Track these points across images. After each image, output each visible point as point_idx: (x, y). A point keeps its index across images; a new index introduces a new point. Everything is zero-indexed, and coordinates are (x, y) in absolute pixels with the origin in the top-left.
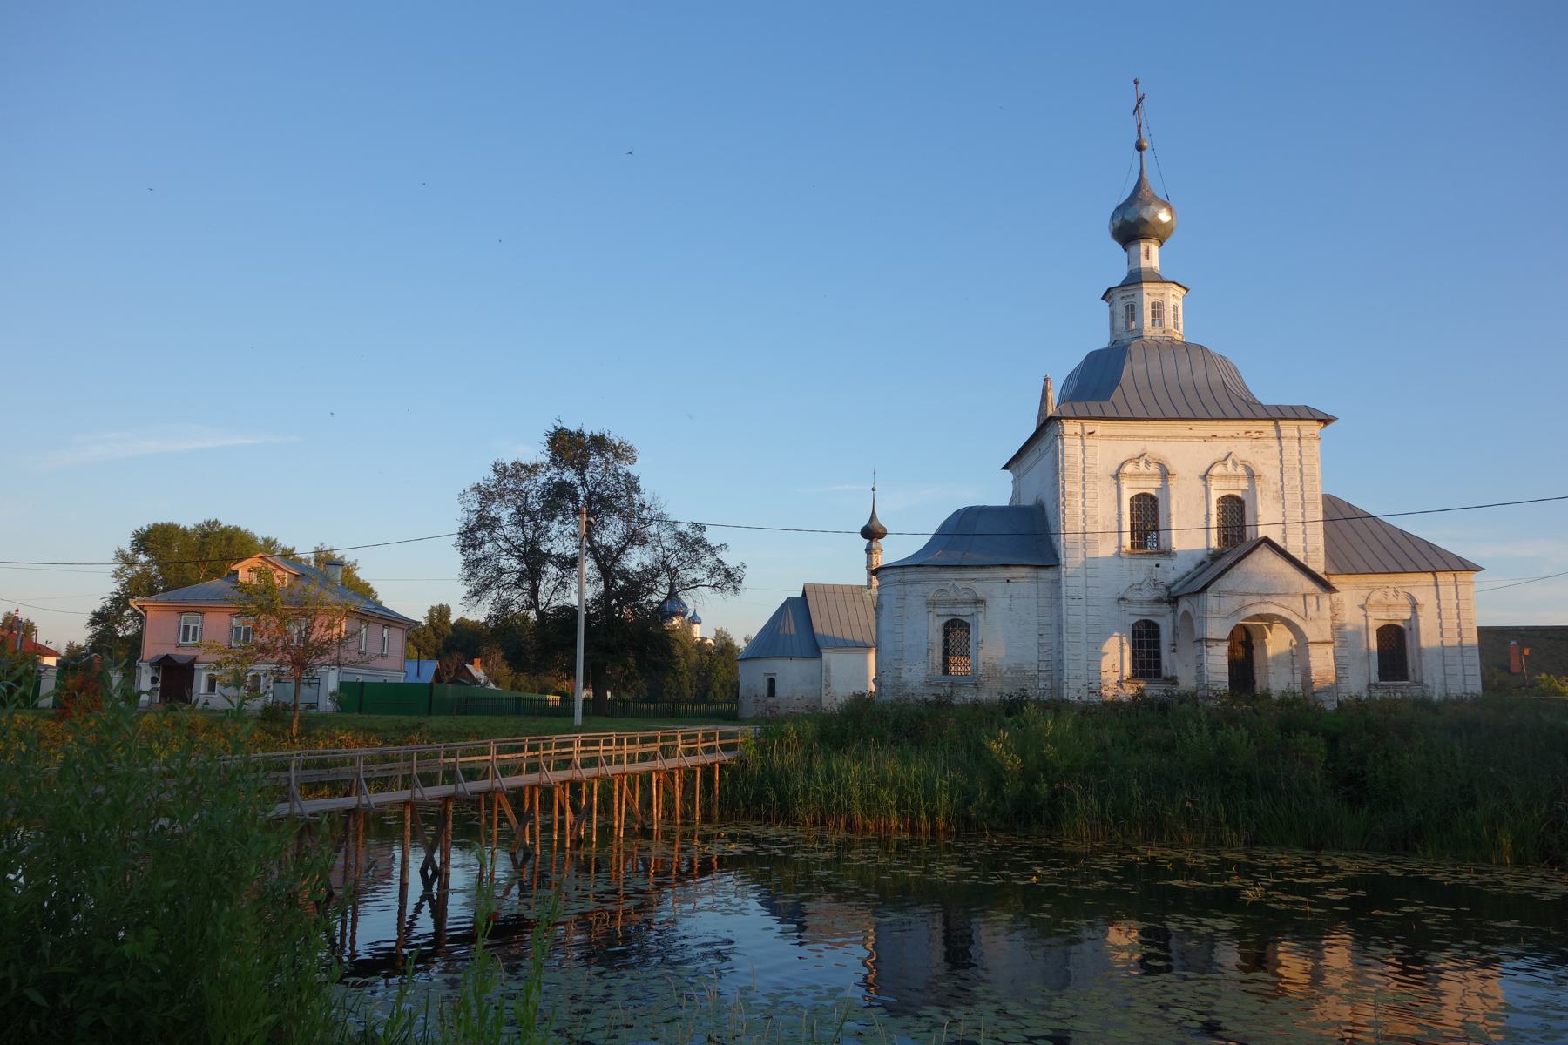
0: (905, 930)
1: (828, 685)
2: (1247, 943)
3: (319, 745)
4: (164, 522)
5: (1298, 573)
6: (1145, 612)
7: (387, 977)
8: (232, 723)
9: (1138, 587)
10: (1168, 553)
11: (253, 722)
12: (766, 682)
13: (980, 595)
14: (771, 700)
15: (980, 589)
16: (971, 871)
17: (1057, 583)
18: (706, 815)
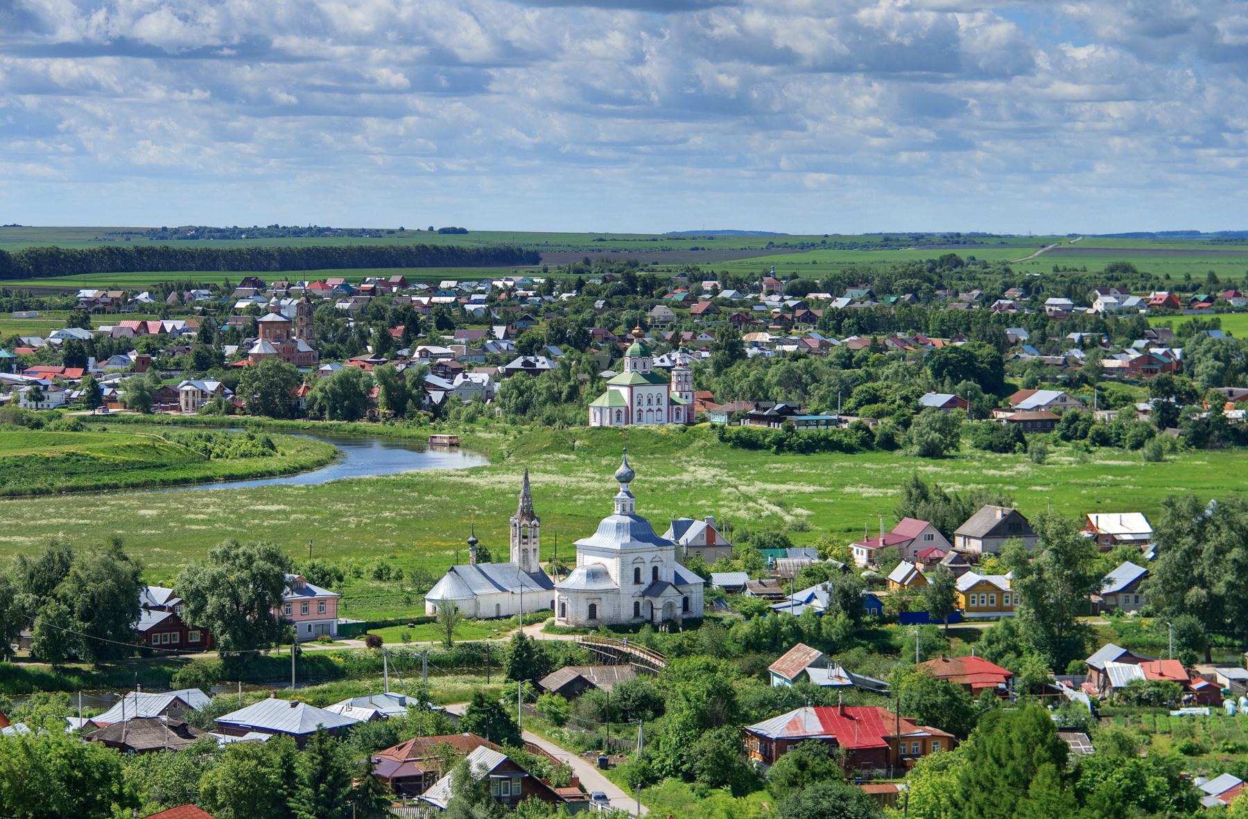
2: (1036, 491)
3: (68, 633)
4: (199, 248)
5: (562, 9)
6: (636, 599)
7: (601, 428)
8: (32, 630)
11: (417, 50)
12: (633, 606)
14: (439, 620)
16: (476, 471)
18: (380, 717)
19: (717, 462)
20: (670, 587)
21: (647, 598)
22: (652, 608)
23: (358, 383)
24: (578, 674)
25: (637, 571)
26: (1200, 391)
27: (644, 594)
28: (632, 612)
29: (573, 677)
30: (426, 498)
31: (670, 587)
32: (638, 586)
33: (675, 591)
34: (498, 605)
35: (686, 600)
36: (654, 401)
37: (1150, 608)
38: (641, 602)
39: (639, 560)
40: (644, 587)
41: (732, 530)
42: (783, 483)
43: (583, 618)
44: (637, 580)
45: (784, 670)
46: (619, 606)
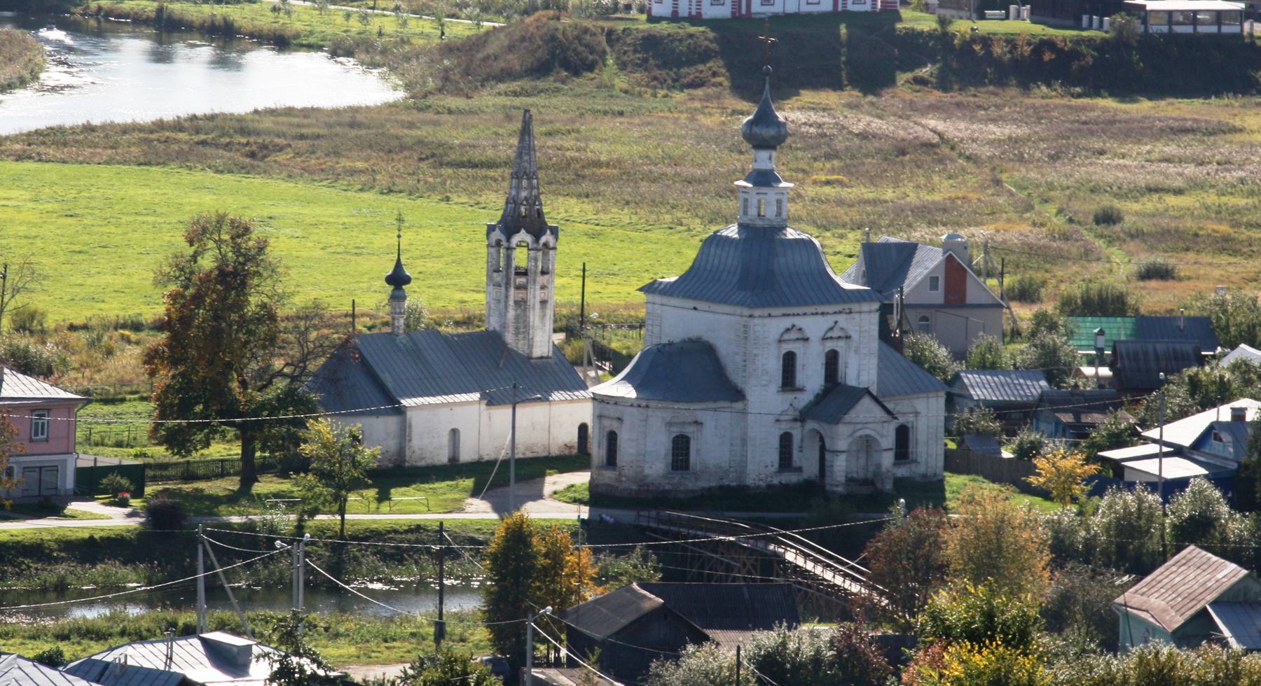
0: (26, 237)
1: (410, 440)
6: (785, 427)
9: (783, 413)
10: (801, 390)
12: (775, 443)
13: (699, 420)
15: (701, 416)
17: (744, 412)
20: (866, 402)
21: (811, 425)
22: (823, 449)
25: (789, 361)
26: (617, 92)
27: (803, 416)
28: (773, 457)
31: (866, 402)
32: (790, 396)
33: (878, 413)
35: (903, 434)
37: (360, 187)
38: (797, 434)
39: (793, 335)
40: (805, 399)
44: (789, 380)
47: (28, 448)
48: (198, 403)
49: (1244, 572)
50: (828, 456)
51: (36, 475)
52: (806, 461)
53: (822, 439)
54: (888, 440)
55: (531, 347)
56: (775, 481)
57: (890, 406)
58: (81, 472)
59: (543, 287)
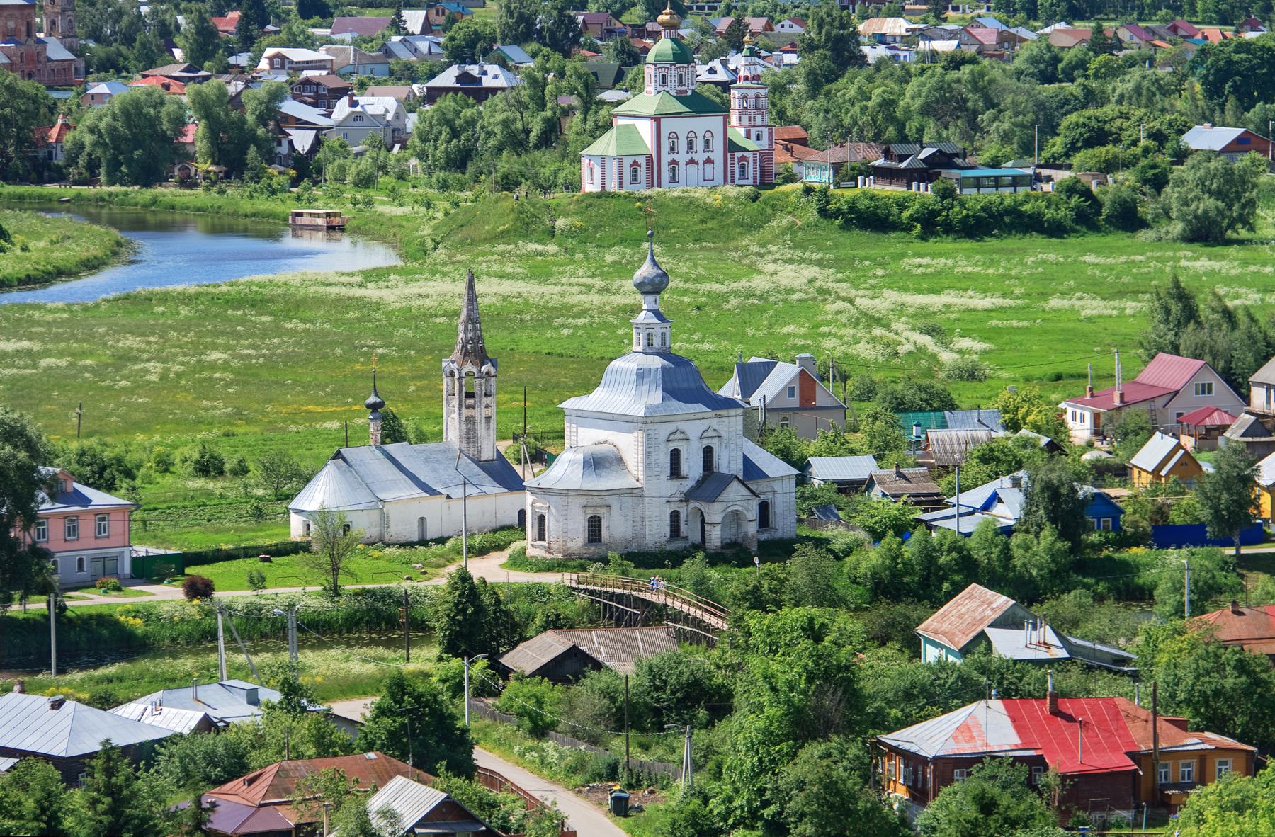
6: (674, 507)
14: (315, 547)
19: (815, 256)
20: (735, 485)
22: (703, 522)
23: (158, 118)
24: (570, 644)
25: (675, 455)
27: (688, 497)
29: (562, 649)
30: (288, 326)
31: (735, 485)
32: (676, 483)
33: (744, 491)
34: (422, 520)
35: (764, 508)
36: (700, 144)
39: (678, 436)
40: (687, 485)
41: (845, 378)
42: (96, 668)
43: (577, 541)
44: (675, 473)
45: (944, 634)
46: (643, 519)
47: (94, 543)
48: (149, 382)
49: (1012, 602)
50: (707, 527)
51: (101, 563)
52: (690, 531)
53: (702, 515)
54: (752, 512)
55: (479, 452)
56: (668, 548)
57: (753, 487)
58: (136, 561)
59: (487, 407)
